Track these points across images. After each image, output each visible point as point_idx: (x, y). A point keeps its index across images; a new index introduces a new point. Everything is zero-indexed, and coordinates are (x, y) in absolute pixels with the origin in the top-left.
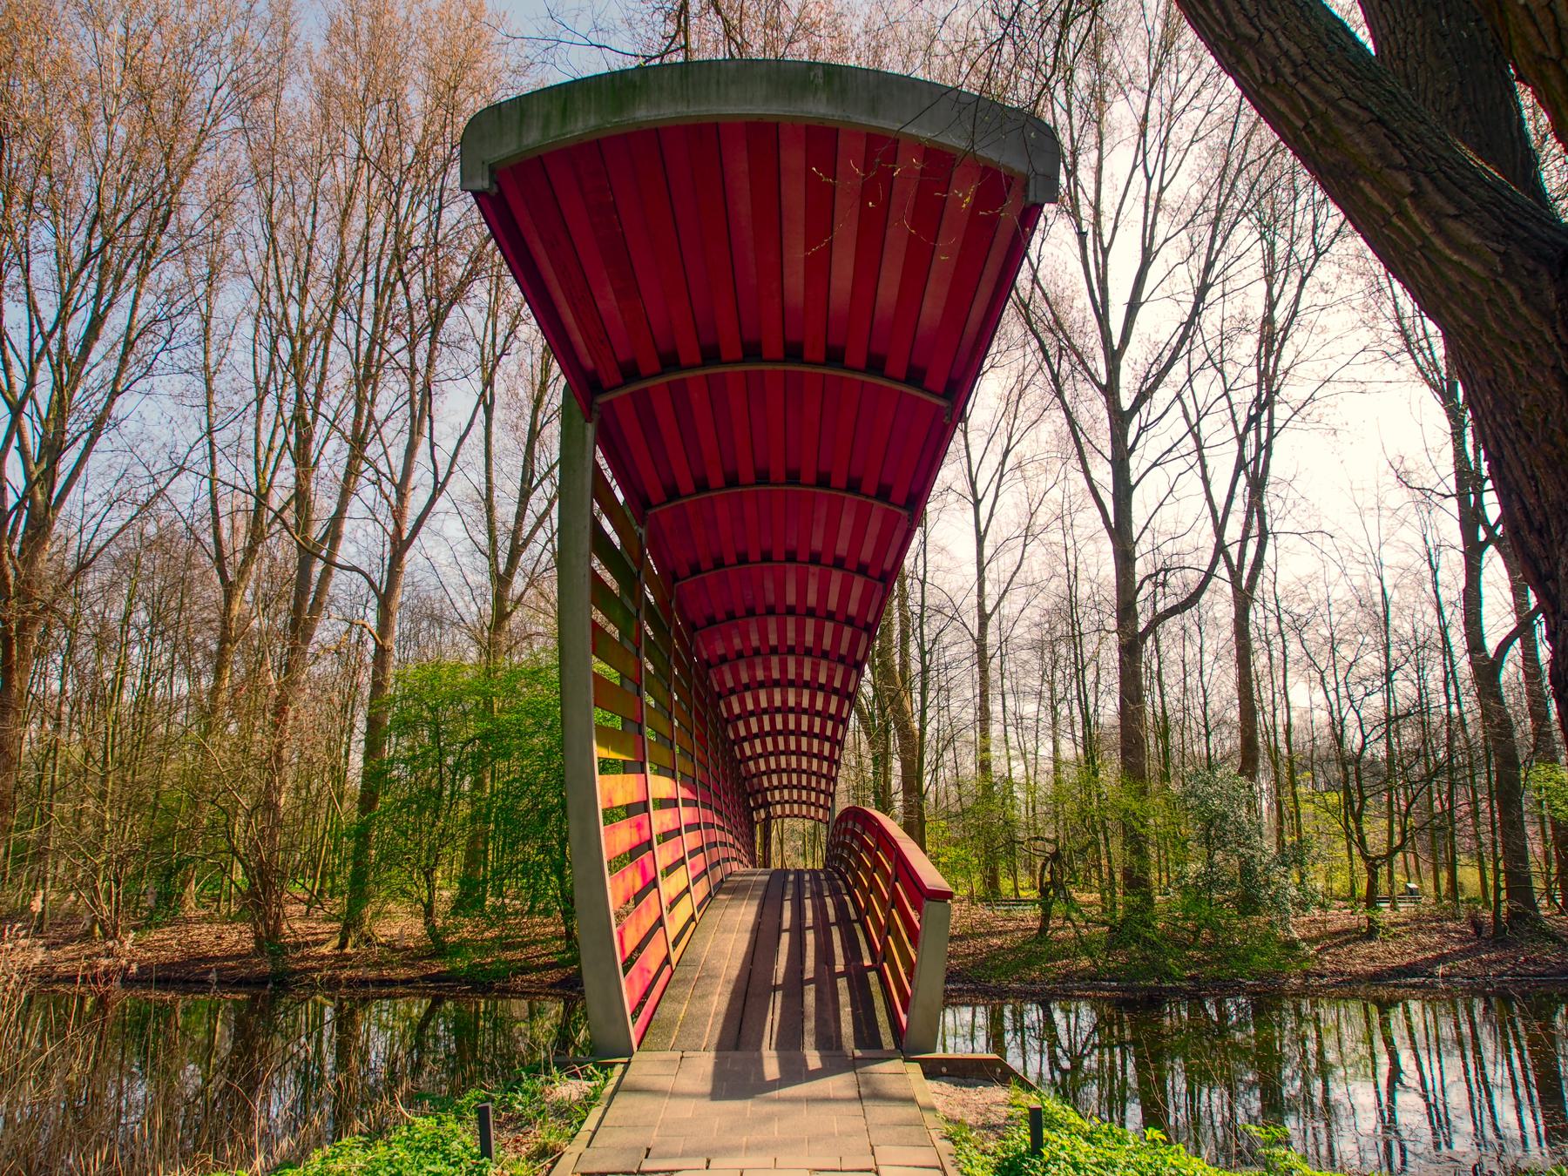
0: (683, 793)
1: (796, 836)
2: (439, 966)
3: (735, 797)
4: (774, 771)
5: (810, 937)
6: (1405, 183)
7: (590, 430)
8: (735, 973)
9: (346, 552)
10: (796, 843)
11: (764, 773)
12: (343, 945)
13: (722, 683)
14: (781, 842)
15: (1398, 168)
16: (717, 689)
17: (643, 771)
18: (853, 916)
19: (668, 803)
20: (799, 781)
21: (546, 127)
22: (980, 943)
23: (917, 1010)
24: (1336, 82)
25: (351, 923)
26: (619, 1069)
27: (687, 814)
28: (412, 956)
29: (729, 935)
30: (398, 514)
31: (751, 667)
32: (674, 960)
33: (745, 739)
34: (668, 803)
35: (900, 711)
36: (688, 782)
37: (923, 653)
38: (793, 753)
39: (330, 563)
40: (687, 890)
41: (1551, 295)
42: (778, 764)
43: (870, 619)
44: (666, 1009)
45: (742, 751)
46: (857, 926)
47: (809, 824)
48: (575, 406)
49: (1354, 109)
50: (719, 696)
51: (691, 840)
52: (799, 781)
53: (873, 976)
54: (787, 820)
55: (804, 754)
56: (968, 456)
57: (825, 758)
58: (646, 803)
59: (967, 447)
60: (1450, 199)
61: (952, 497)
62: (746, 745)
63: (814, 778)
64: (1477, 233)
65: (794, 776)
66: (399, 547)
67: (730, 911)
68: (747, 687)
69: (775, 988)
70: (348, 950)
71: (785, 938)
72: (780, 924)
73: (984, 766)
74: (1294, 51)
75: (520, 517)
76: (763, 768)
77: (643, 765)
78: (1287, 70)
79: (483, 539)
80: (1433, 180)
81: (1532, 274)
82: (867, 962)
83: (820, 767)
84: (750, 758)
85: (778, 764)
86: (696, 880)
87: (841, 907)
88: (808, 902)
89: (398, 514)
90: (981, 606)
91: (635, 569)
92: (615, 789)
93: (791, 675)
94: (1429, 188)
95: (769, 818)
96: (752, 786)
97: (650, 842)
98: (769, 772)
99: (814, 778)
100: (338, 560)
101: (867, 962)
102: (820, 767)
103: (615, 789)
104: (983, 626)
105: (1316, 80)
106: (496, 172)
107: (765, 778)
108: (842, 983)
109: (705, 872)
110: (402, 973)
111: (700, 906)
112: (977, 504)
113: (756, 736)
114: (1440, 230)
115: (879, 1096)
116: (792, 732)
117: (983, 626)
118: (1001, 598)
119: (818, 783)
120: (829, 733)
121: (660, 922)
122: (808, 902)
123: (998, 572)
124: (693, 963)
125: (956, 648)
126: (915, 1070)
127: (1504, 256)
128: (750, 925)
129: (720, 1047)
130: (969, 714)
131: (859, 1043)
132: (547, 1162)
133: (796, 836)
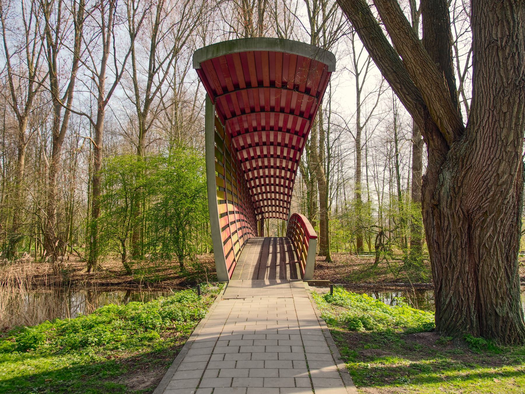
0: (236, 209)
1: (274, 227)
2: (129, 278)
3: (253, 211)
4: (265, 200)
5: (279, 255)
6: (399, 86)
7: (214, 106)
8: (255, 264)
9: (75, 104)
10: (274, 227)
11: (261, 200)
12: (89, 271)
13: (246, 168)
14: (268, 229)
15: (398, 83)
16: (244, 169)
17: (226, 203)
18: (293, 249)
19: (232, 213)
20: (276, 203)
21: (213, 54)
22: (350, 269)
23: (307, 269)
24: (387, 63)
25: (91, 263)
26: (226, 284)
27: (237, 216)
28: (118, 275)
29: (252, 254)
30: (100, 88)
31: (257, 161)
32: (236, 260)
33: (254, 187)
34: (232, 213)
35: (319, 173)
36: (237, 205)
37: (328, 149)
38: (273, 192)
39: (68, 110)
40: (238, 241)
41: (423, 113)
42: (267, 197)
43: (300, 146)
44: (235, 272)
45: (252, 192)
46: (294, 252)
47: (280, 221)
48: (209, 100)
49: (390, 69)
50: (245, 172)
51: (238, 225)
52: (276, 203)
53: (297, 264)
54: (270, 220)
55: (277, 193)
56: (354, 53)
57: (286, 194)
58: (227, 212)
59: (353, 48)
60: (407, 91)
61: (346, 72)
62: (254, 190)
63: (281, 202)
64: (411, 98)
65: (273, 187)
66: (102, 104)
67: (251, 249)
68: (255, 169)
69: (268, 267)
70: (91, 273)
71: (270, 256)
72: (269, 252)
73: (358, 196)
74: (379, 54)
75: (149, 87)
76: (261, 198)
77: (226, 201)
78: (378, 58)
79: (132, 94)
80: (404, 86)
81: (420, 108)
82: (296, 261)
83: (284, 198)
84: (255, 195)
85: (267, 197)
86: (240, 238)
87: (289, 247)
88: (278, 246)
89: (100, 88)
90: (358, 123)
91: (222, 139)
92: (221, 209)
93: (272, 164)
94: (403, 88)
95: (263, 218)
96: (256, 206)
97: (228, 224)
98: (263, 200)
99: (281, 202)
100: (72, 108)
101: (296, 261)
102: (284, 198)
103: (221, 209)
104: (359, 134)
105: (383, 61)
106: (201, 64)
107: (261, 202)
108: (288, 266)
109: (242, 236)
110: (116, 281)
111: (242, 247)
112: (357, 75)
113: (258, 186)
114: (405, 97)
115: (294, 287)
116: (272, 185)
117: (359, 134)
118: (367, 121)
119: (283, 204)
120: (287, 185)
121: (232, 249)
122: (278, 246)
123: (365, 110)
124: (242, 262)
125: (347, 144)
126: (306, 284)
127: (416, 104)
128: (259, 252)
129: (253, 279)
130: (352, 172)
131: (291, 278)
132: (214, 299)
133: (274, 227)
